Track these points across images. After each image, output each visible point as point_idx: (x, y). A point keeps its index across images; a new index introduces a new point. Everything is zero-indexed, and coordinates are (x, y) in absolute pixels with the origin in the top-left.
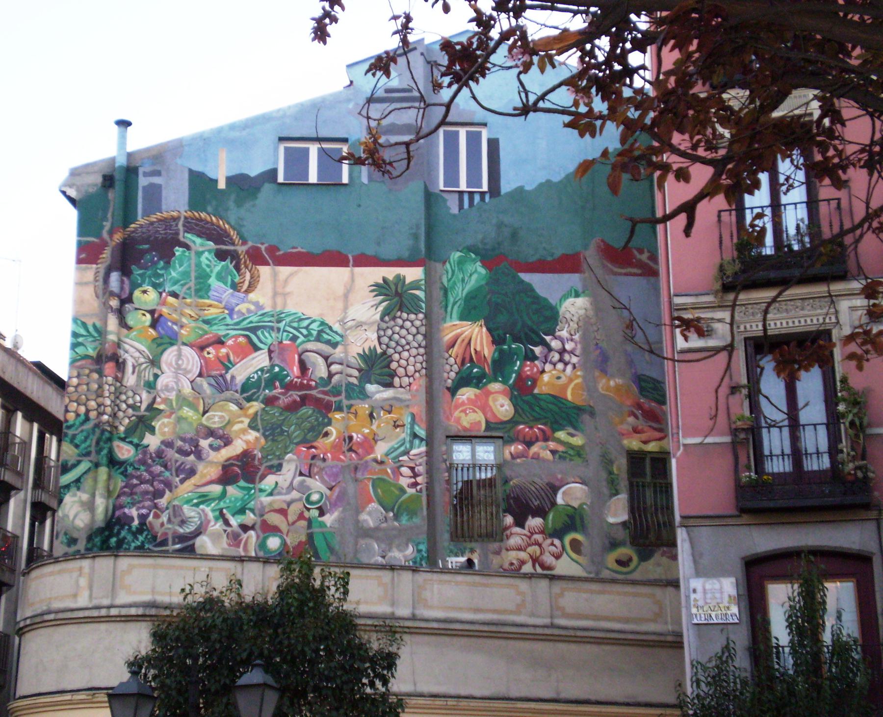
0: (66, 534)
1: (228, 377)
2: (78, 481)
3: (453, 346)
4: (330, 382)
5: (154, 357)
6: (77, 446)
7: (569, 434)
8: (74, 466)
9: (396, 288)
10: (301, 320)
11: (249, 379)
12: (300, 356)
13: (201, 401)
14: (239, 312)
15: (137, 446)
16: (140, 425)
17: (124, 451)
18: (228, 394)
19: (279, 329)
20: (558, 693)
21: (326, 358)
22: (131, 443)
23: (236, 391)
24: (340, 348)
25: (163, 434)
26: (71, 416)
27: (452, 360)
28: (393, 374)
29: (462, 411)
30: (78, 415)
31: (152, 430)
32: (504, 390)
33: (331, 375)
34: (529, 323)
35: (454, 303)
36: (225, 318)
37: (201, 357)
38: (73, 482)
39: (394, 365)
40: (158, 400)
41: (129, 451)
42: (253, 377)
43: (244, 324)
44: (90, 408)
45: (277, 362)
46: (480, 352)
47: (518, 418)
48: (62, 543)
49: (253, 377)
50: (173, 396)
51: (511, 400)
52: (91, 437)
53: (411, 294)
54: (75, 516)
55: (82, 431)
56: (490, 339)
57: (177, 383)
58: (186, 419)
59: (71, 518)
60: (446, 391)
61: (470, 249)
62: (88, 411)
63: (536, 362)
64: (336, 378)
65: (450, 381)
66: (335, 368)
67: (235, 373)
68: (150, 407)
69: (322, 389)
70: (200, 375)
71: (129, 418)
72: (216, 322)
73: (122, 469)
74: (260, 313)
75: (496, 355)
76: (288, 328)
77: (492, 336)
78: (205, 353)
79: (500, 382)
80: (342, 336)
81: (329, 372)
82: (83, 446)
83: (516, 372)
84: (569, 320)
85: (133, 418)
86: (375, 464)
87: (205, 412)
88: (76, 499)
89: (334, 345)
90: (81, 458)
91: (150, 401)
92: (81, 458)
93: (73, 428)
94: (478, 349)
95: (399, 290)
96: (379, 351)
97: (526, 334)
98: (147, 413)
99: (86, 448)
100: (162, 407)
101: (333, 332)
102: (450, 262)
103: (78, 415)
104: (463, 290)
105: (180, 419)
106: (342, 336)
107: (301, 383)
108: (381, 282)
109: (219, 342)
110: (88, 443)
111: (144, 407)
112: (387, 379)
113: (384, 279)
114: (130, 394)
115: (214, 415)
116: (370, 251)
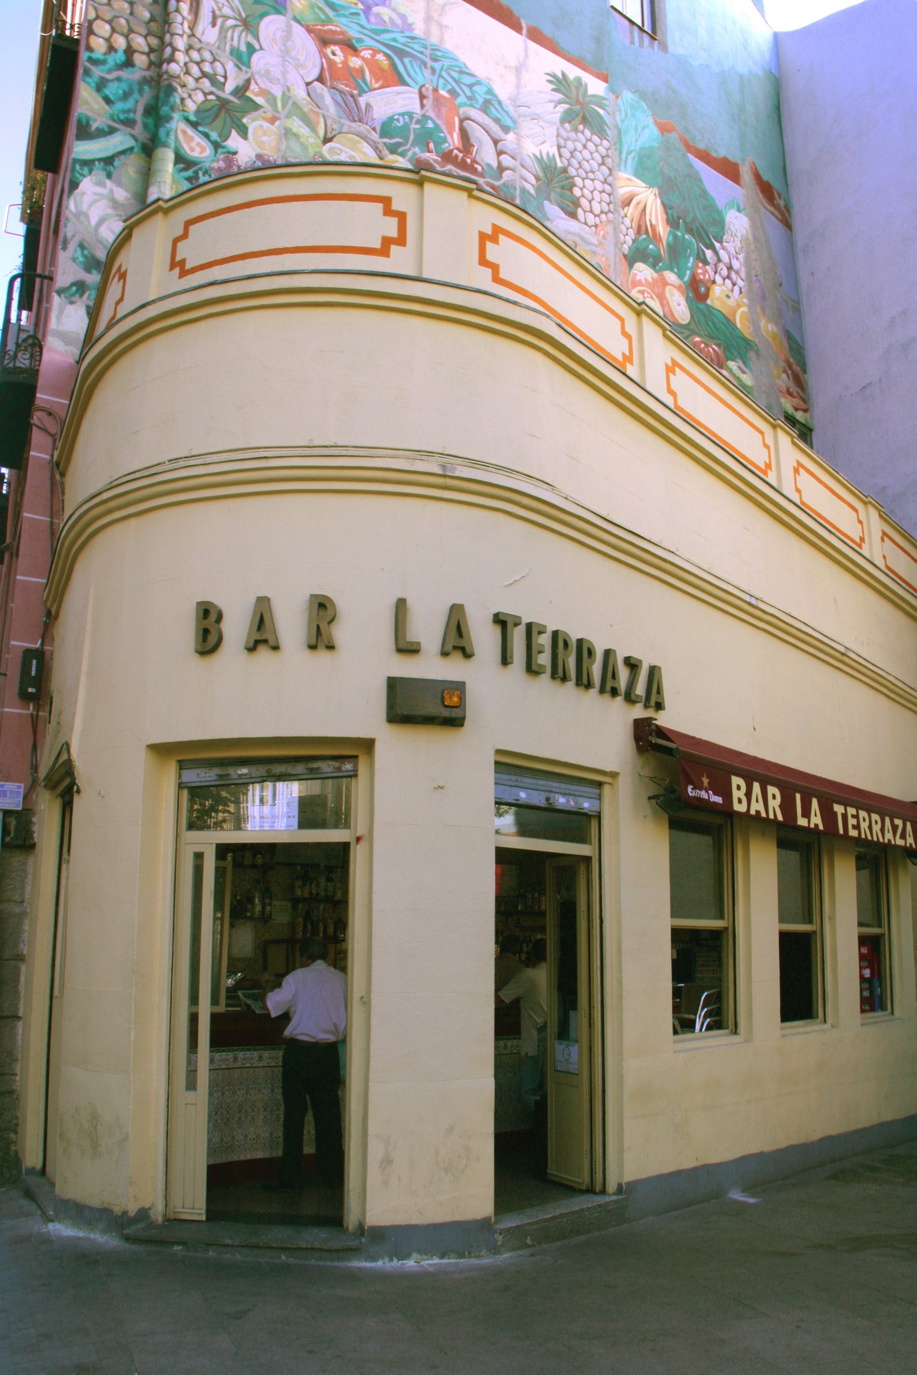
0: (82, 246)
1: (362, 101)
2: (108, 161)
3: (628, 204)
4: (501, 177)
5: (247, 16)
6: (108, 101)
7: (740, 368)
8: (101, 133)
9: (577, 94)
10: (461, 72)
11: (391, 119)
12: (461, 121)
13: (322, 120)
14: (378, 15)
15: (216, 146)
16: (222, 114)
17: (193, 144)
18: (363, 128)
19: (433, 71)
20: (113, 232)
21: (496, 142)
22: (207, 136)
23: (374, 129)
24: (511, 137)
25: (261, 144)
26: (99, 44)
27: (627, 221)
28: (576, 204)
29: (639, 292)
30: (111, 49)
31: (243, 132)
32: (681, 285)
33: (501, 169)
34: (701, 220)
35: (629, 153)
36: (357, 14)
37: (323, 55)
38: (100, 160)
39: (577, 192)
40: (253, 86)
41: (203, 150)
42: (398, 120)
43: (385, 37)
44: (135, 46)
45: (431, 114)
46: (655, 226)
47: (692, 326)
48: (74, 260)
49: (398, 120)
50: (278, 92)
51: (687, 301)
52: (136, 96)
53: (593, 108)
54: (101, 222)
55: (119, 79)
56: (665, 217)
57: (284, 75)
58: (297, 136)
59: (94, 221)
60: (622, 257)
61: (643, 95)
62: (130, 51)
63: (707, 267)
64: (507, 174)
65: (625, 246)
66: (506, 160)
67: (372, 101)
68: (241, 91)
69: (491, 181)
70: (320, 79)
71: (205, 94)
72: (346, 13)
73: (190, 173)
74: (407, 34)
75: (671, 239)
76: (444, 74)
77: (667, 213)
78: (328, 51)
79: (675, 272)
80: (514, 122)
81: (499, 163)
82: (120, 106)
83: (690, 269)
84: (733, 234)
85: (211, 97)
86: (767, 313)
87: (326, 140)
88: (105, 192)
89: (506, 129)
90: (117, 126)
91: (241, 82)
92: (117, 126)
93: (102, 67)
94: (654, 222)
95: (581, 99)
96: (559, 164)
97: (697, 228)
98: (232, 98)
99: (124, 112)
100: (259, 100)
101: (503, 110)
102: (622, 98)
103: (111, 49)
104: (636, 141)
105: (288, 133)
106: (514, 122)
107: (463, 160)
108: (560, 76)
109: (350, 47)
110: (129, 104)
111: (230, 86)
112: (571, 208)
113: (563, 74)
114: (207, 55)
115: (341, 151)
116: (547, 30)
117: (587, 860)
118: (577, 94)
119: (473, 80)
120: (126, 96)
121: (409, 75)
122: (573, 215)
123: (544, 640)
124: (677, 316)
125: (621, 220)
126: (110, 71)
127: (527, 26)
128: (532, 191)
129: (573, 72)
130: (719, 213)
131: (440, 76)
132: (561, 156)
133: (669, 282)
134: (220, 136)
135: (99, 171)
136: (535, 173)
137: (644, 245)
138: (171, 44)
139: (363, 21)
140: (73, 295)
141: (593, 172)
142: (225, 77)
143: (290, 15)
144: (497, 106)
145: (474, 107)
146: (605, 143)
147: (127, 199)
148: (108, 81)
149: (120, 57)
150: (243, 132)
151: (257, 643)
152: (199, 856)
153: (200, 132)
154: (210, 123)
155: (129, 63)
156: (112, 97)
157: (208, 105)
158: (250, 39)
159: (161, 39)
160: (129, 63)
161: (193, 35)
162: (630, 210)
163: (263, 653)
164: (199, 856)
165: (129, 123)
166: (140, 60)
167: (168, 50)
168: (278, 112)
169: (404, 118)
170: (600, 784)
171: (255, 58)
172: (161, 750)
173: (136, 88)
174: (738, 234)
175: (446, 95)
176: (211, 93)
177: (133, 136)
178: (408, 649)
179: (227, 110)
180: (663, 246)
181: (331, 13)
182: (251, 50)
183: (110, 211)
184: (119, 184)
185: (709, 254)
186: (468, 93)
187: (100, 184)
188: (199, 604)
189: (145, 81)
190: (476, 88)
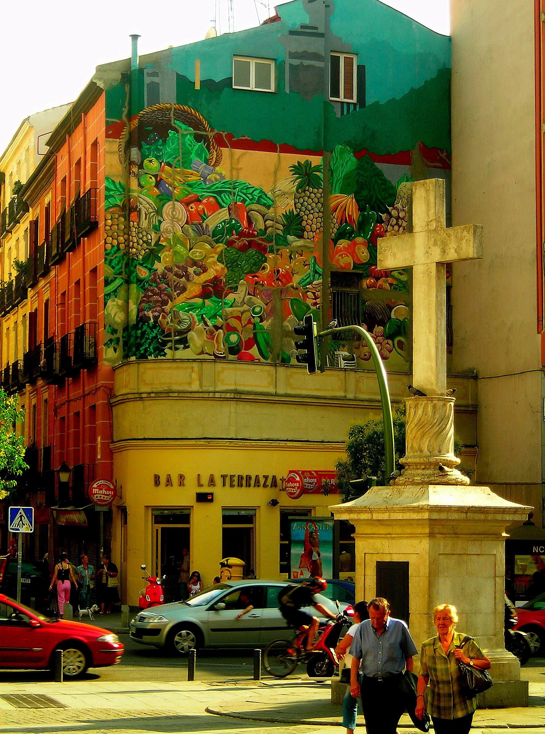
2: (115, 291)
6: (113, 268)
9: (306, 170)
12: (247, 214)
13: (188, 241)
15: (150, 270)
17: (142, 273)
21: (263, 216)
22: (146, 267)
23: (209, 236)
25: (166, 262)
28: (303, 230)
30: (113, 246)
33: (266, 228)
37: (187, 210)
38: (112, 292)
40: (162, 238)
41: (146, 273)
62: (119, 244)
70: (187, 223)
71: (145, 250)
72: (196, 186)
73: (142, 285)
76: (240, 194)
79: (362, 236)
81: (265, 225)
82: (117, 267)
85: (147, 250)
88: (115, 303)
89: (268, 207)
90: (116, 276)
92: (116, 276)
98: (155, 248)
103: (113, 246)
105: (175, 253)
106: (273, 201)
111: (153, 244)
114: (145, 233)
117: (253, 528)
118: (306, 170)
119: (252, 190)
120: (118, 264)
121: (224, 202)
122: (301, 237)
123: (236, 479)
124: (361, 260)
125: (331, 221)
126: (113, 256)
127: (279, 145)
128: (281, 233)
129: (302, 158)
130: (393, 188)
131: (238, 195)
132: (296, 208)
133: (358, 243)
134: (151, 266)
135: (113, 297)
136: (282, 223)
137: (344, 228)
138: (132, 241)
139: (203, 186)
140: (109, 345)
141: (313, 209)
142: (151, 240)
143: (174, 199)
144: (264, 197)
145: (254, 203)
146: (321, 190)
147: (122, 303)
148: (112, 260)
149: (116, 248)
150: (159, 260)
151: (167, 485)
152: (157, 530)
153: (144, 267)
154: (147, 261)
155: (119, 249)
156: (114, 266)
157: (147, 253)
158: (160, 218)
159: (128, 234)
160: (119, 249)
161: (139, 227)
162: (336, 214)
163: (169, 487)
164: (157, 530)
165: (120, 274)
166: (122, 246)
167: (131, 243)
168: (171, 246)
169: (222, 224)
170: (256, 509)
171: (162, 225)
172: (147, 507)
173: (121, 258)
174: (405, 196)
175: (240, 203)
176: (147, 249)
177: (122, 278)
178: (200, 485)
179: (153, 254)
180: (355, 225)
181: (189, 189)
182: (160, 222)
183: (117, 310)
184: (119, 299)
185: (384, 216)
186: (251, 197)
187: (114, 301)
188: (154, 475)
189: (125, 254)
190: (255, 193)
